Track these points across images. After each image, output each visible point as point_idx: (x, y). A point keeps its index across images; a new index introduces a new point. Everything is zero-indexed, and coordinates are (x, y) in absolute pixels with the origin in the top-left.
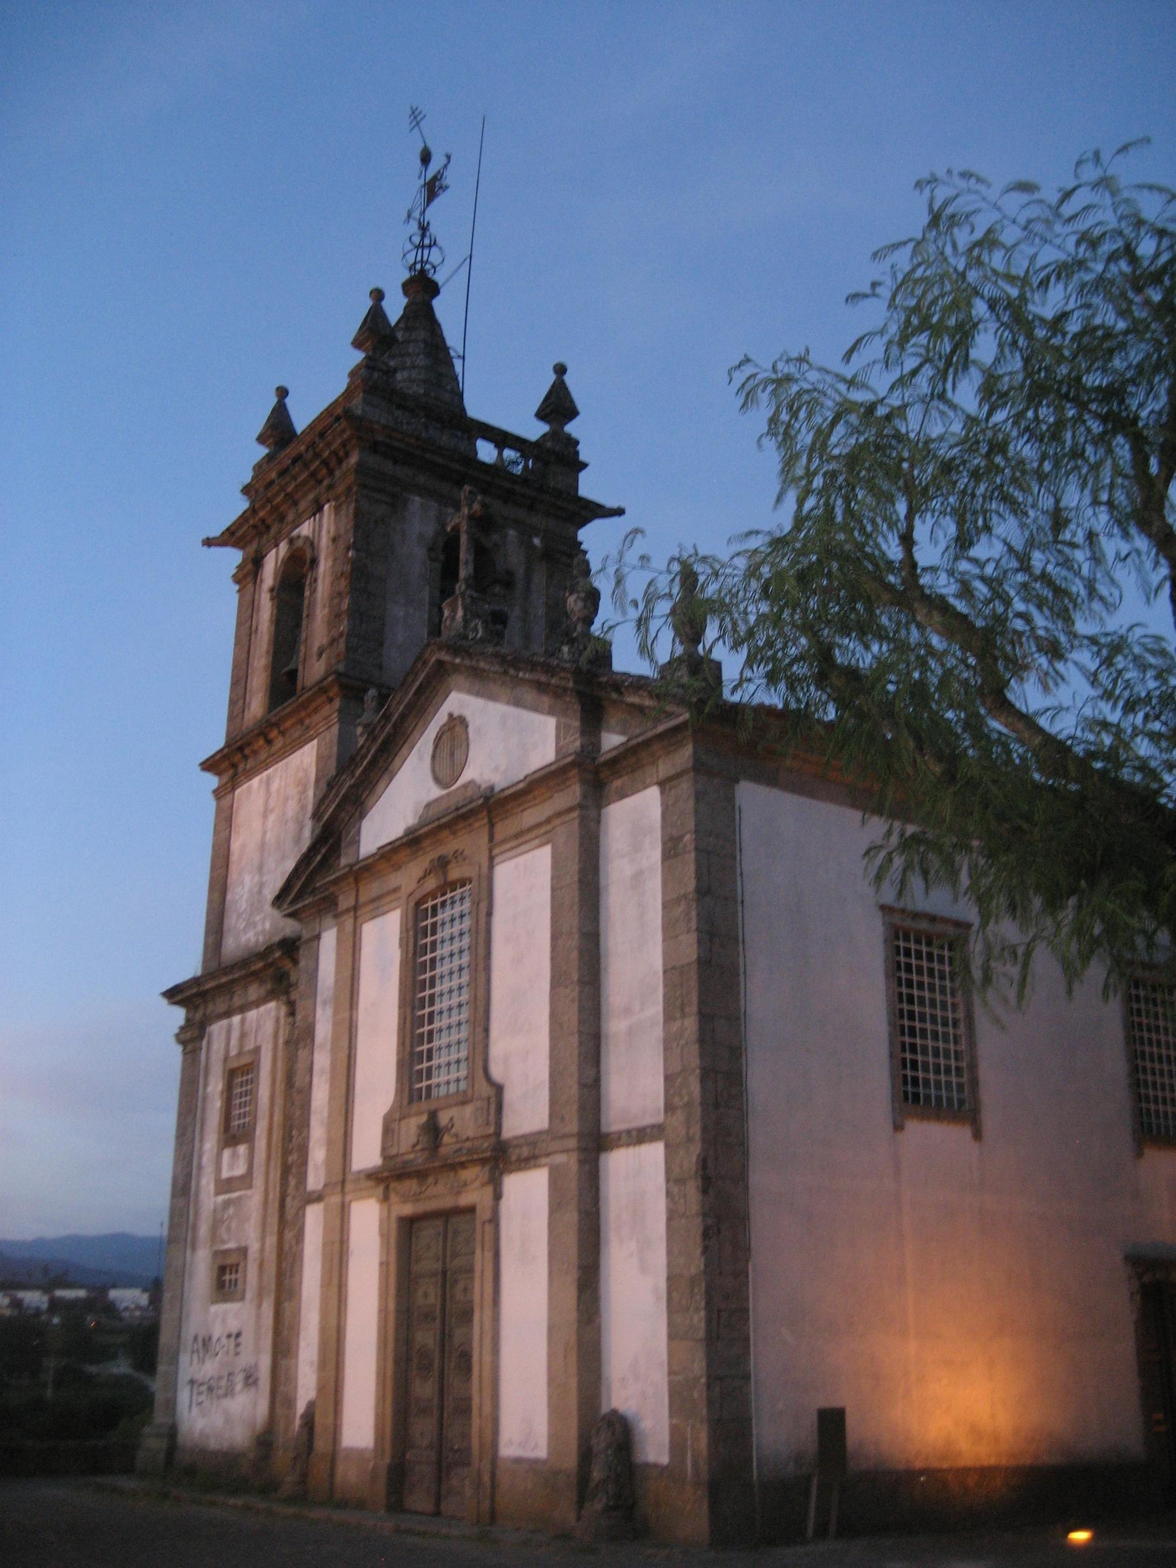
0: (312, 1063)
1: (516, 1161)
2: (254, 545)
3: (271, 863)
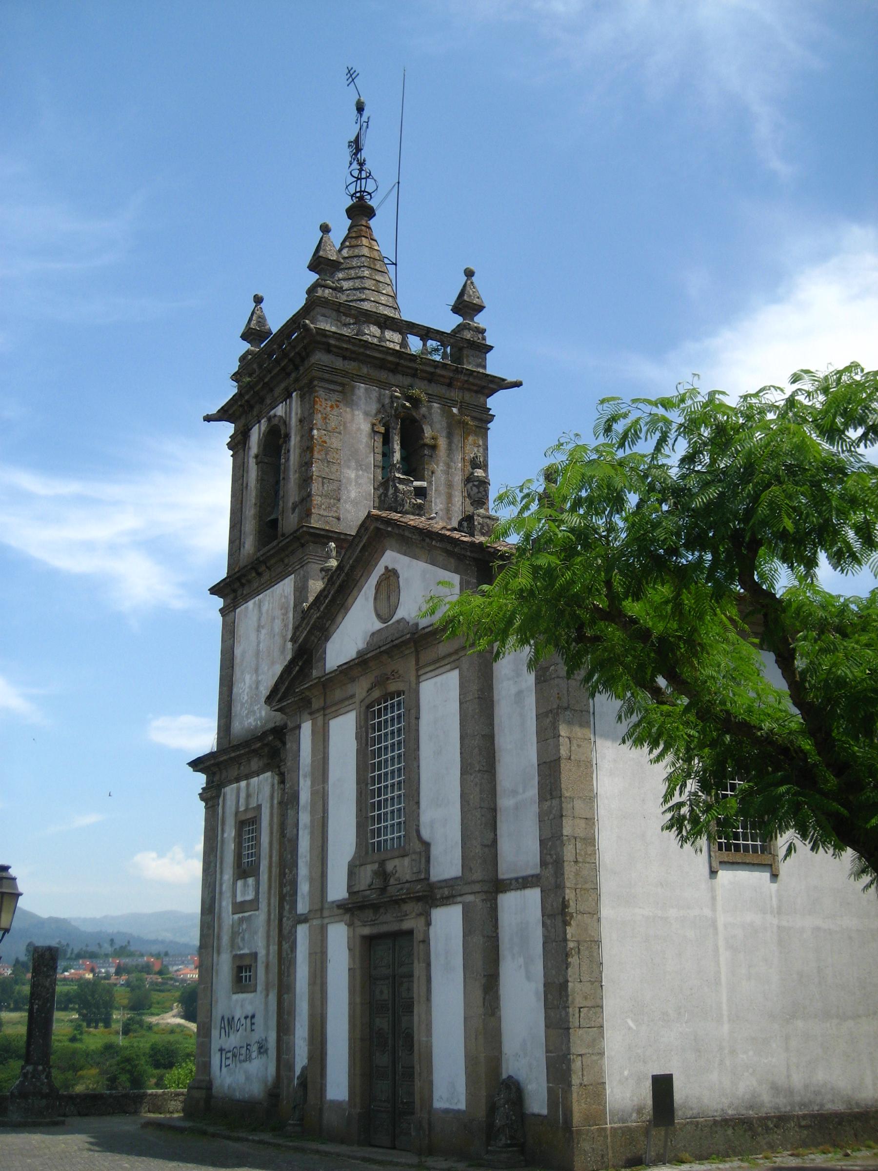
0: (298, 820)
1: (440, 899)
2: (242, 421)
3: (264, 667)
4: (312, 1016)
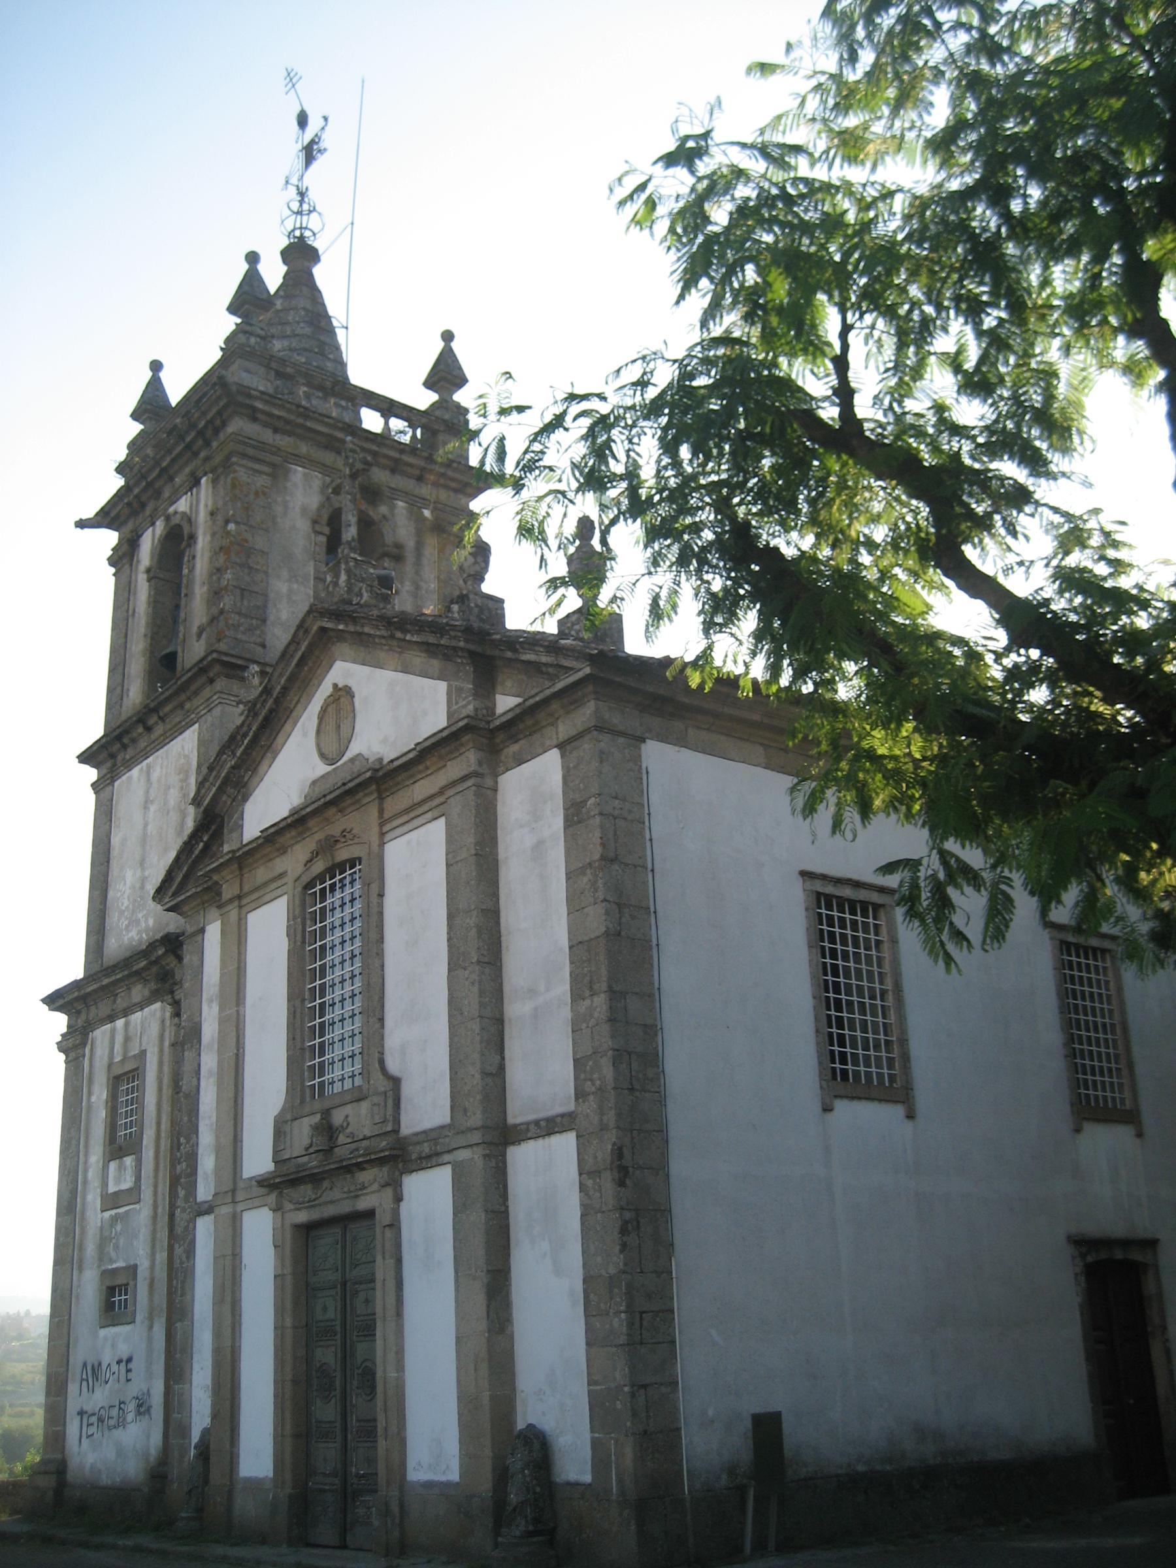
2: (130, 525)
4: (217, 1351)
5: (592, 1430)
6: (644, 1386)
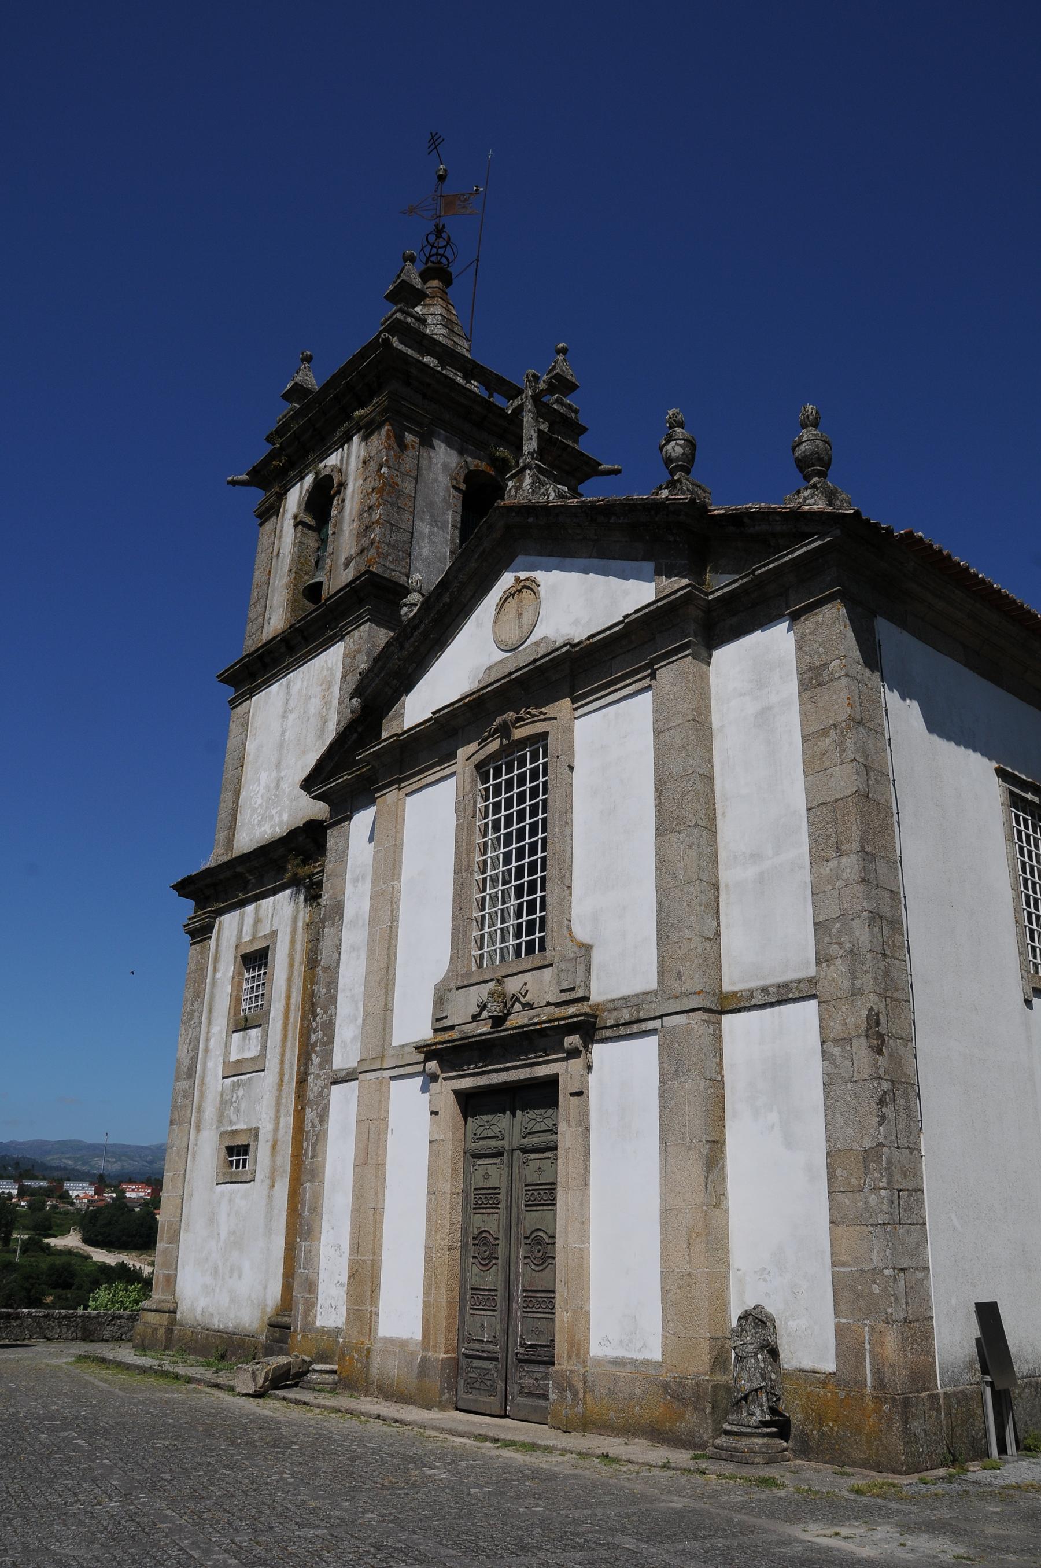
5: (837, 1315)
6: (903, 1270)
